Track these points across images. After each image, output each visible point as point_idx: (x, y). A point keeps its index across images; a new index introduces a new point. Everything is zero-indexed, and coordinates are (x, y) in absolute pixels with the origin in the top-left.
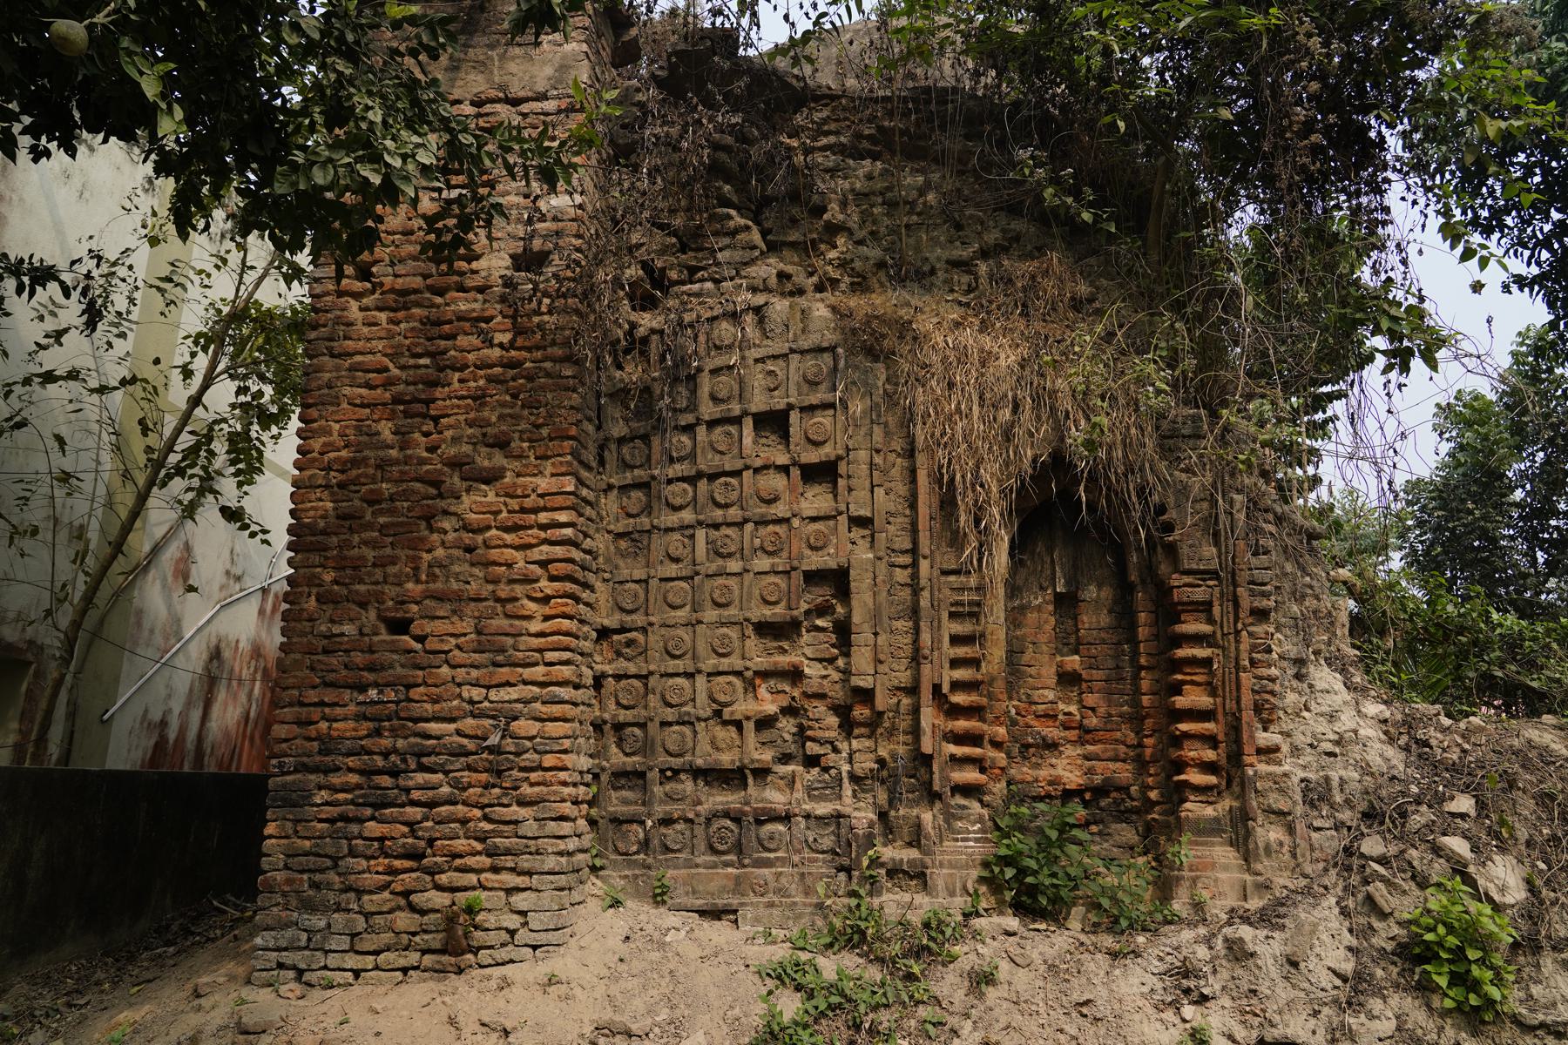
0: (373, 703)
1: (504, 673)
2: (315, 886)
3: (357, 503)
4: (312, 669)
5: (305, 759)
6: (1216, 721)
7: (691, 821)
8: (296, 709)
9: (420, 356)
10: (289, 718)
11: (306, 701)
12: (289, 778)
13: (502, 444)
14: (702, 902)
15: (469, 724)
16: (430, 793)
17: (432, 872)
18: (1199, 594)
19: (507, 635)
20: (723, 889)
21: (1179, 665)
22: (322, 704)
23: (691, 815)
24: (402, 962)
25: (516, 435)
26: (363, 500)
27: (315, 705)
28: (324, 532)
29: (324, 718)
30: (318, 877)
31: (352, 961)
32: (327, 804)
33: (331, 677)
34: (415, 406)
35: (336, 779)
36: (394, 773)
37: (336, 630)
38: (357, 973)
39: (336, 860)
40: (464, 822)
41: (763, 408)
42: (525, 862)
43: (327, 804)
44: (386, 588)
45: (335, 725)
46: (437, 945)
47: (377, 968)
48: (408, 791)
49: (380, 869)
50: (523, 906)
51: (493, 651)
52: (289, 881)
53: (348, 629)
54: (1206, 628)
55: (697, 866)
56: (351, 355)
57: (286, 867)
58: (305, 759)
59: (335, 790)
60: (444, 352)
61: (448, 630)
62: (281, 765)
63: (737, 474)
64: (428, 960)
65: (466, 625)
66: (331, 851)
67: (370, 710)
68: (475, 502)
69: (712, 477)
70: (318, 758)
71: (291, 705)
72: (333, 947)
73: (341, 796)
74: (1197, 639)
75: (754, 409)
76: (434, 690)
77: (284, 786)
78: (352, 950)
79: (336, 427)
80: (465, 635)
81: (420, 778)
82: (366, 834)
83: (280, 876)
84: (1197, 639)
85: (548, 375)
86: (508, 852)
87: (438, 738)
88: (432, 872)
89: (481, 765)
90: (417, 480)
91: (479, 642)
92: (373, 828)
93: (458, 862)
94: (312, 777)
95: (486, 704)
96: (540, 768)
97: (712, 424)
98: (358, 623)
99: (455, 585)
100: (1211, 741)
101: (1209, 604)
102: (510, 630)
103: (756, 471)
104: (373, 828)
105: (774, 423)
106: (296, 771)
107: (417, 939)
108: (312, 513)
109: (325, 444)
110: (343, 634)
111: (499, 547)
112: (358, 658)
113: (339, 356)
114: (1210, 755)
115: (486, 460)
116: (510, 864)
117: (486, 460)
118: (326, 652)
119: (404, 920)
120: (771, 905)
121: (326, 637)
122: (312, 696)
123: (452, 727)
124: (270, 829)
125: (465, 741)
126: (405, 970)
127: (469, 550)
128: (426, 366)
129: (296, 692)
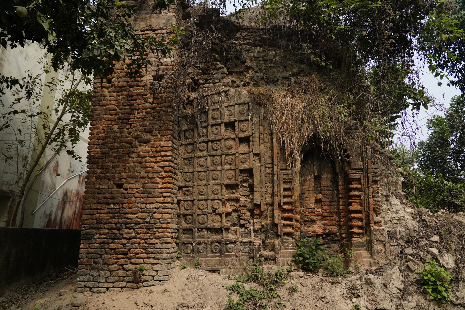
0: (112, 208)
1: (151, 200)
2: (95, 263)
3: (107, 149)
4: (94, 198)
5: (92, 225)
7: (206, 244)
9: (126, 106)
10: (87, 213)
11: (92, 208)
12: (87, 231)
13: (150, 132)
16: (129, 235)
17: (130, 259)
19: (152, 188)
20: (216, 264)
22: (97, 209)
23: (206, 242)
24: (121, 285)
25: (154, 129)
26: (109, 148)
28: (97, 158)
30: (96, 260)
31: (106, 285)
32: (98, 238)
33: (100, 201)
34: (124, 121)
35: (101, 231)
36: (118, 229)
37: (101, 187)
38: (107, 289)
39: (101, 255)
41: (227, 121)
42: (157, 256)
43: (98, 238)
44: (116, 175)
45: (101, 215)
47: (113, 287)
48: (122, 235)
50: (157, 269)
52: (87, 261)
53: (105, 187)
55: (208, 257)
56: (105, 105)
57: (87, 257)
58: (92, 225)
59: (101, 234)
61: (132, 186)
62: (85, 227)
63: (220, 140)
64: (128, 285)
65: (140, 186)
67: (111, 211)
68: (142, 149)
69: (212, 142)
70: (96, 225)
71: (88, 209)
72: (100, 281)
73: (103, 236)
74: (357, 189)
75: (225, 121)
77: (86, 233)
78: (106, 282)
79: (101, 127)
80: (139, 188)
81: (126, 231)
82: (110, 247)
83: (85, 260)
84: (357, 189)
86: (152, 253)
87: (131, 219)
88: (130, 259)
89: (144, 227)
90: (125, 143)
91: (143, 191)
92: (112, 246)
93: (137, 256)
94: (94, 231)
97: (212, 126)
98: (107, 185)
99: (136, 174)
100: (361, 220)
101: (360, 179)
103: (226, 140)
104: (112, 246)
105: (231, 125)
106: (89, 229)
107: (125, 278)
108: (94, 152)
109: (98, 132)
110: (103, 188)
112: (108, 195)
113: (102, 106)
114: (360, 224)
115: (145, 136)
116: (153, 256)
117: (145, 136)
118: (98, 193)
119: (121, 273)
120: (230, 268)
121: (98, 189)
122: (94, 206)
123: (136, 216)
124: (82, 246)
125: (139, 220)
126: (122, 288)
127: (141, 163)
128: (128, 109)
129: (89, 205)
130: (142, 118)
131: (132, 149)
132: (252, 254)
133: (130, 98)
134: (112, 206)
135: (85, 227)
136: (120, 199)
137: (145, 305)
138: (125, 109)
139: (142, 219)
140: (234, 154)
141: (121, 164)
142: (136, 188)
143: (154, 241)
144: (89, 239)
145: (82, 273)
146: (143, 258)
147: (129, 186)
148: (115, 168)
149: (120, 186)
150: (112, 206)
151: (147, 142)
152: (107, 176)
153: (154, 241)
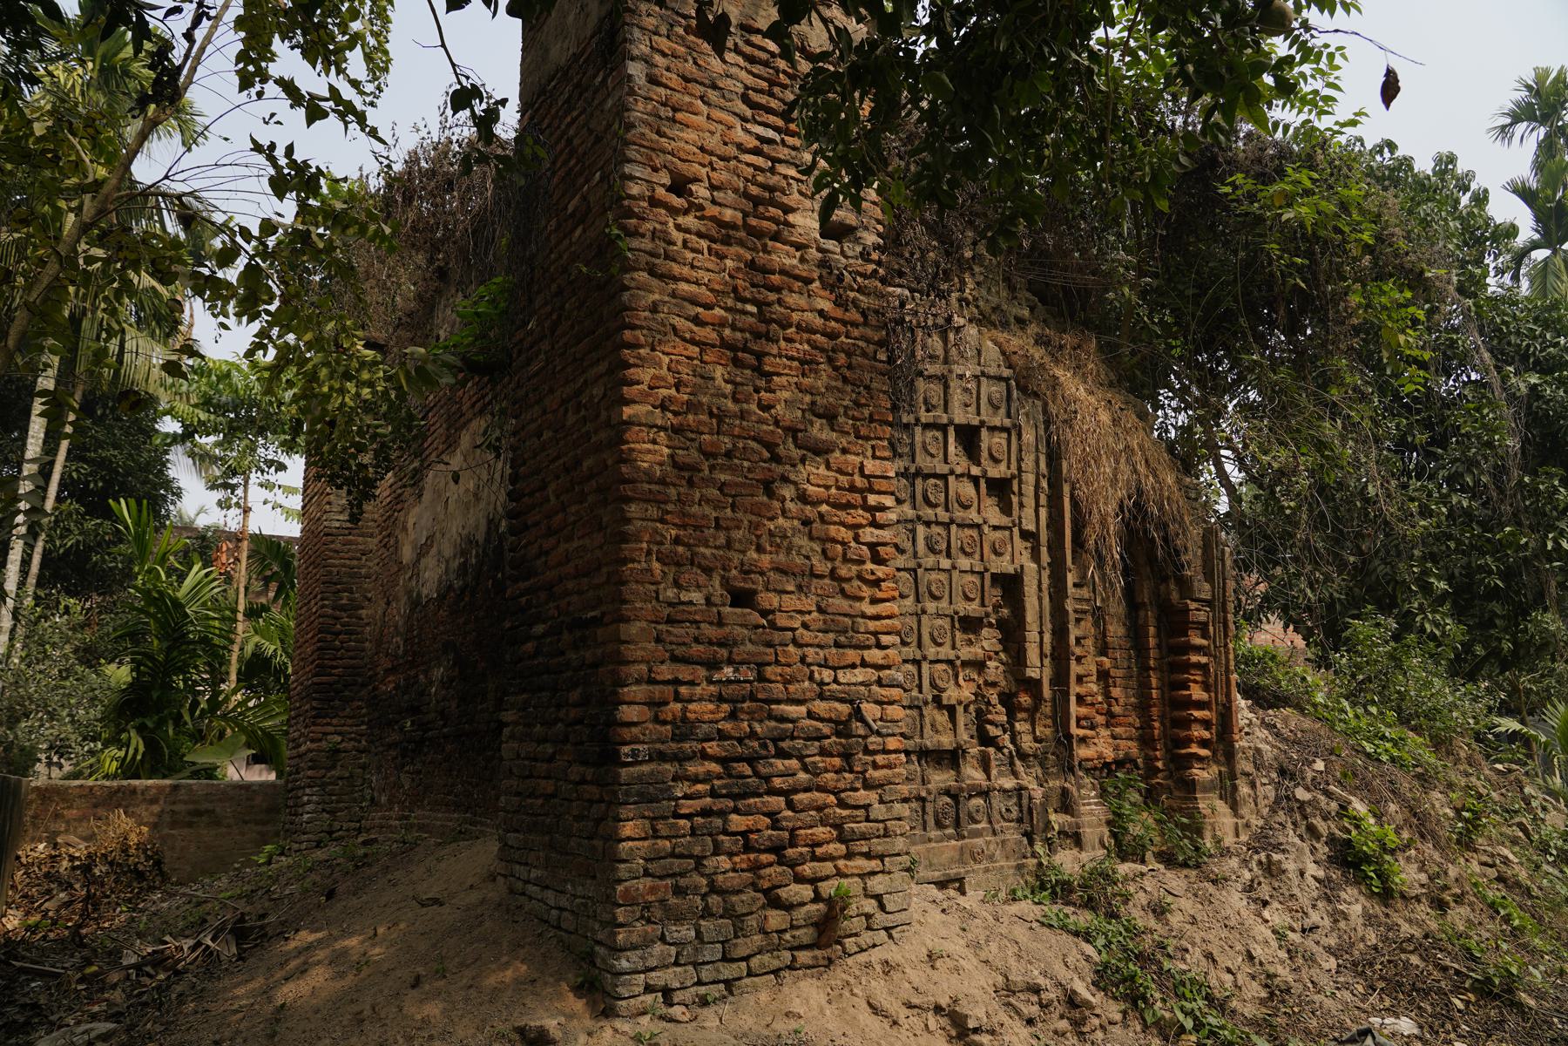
0: (729, 682)
1: (852, 655)
2: (679, 891)
3: (695, 454)
4: (658, 640)
5: (658, 746)
6: (1210, 710)
7: (923, 800)
8: (644, 687)
9: (745, 301)
10: (640, 697)
11: (659, 678)
12: (646, 768)
13: (830, 417)
14: (937, 874)
15: (820, 707)
16: (790, 780)
17: (793, 865)
18: (1202, 616)
19: (845, 615)
20: (952, 860)
21: (1188, 667)
22: (677, 682)
23: (924, 794)
24: (776, 964)
25: (842, 410)
26: (700, 450)
27: (667, 682)
28: (662, 482)
29: (677, 698)
30: (683, 882)
31: (728, 971)
32: (686, 797)
33: (679, 651)
34: (748, 356)
35: (693, 768)
36: (751, 760)
37: (684, 597)
38: (728, 984)
39: (699, 860)
40: (819, 809)
41: (964, 421)
42: (878, 846)
43: (686, 797)
44: (731, 554)
45: (691, 707)
46: (806, 940)
47: (750, 975)
48: (768, 779)
49: (744, 866)
50: (879, 889)
51: (844, 634)
52: (653, 890)
53: (697, 597)
54: (1205, 642)
55: (930, 840)
56: (676, 279)
57: (647, 873)
58: (658, 746)
59: (696, 780)
60: (769, 304)
61: (792, 606)
62: (634, 753)
63: (944, 477)
64: (804, 957)
65: (809, 603)
66: (697, 850)
67: (728, 691)
68: (815, 476)
69: (927, 477)
70: (674, 745)
71: (638, 682)
72: (707, 958)
73: (700, 787)
74: (1199, 649)
75: (957, 421)
76: (788, 670)
77: (640, 778)
78: (726, 959)
79: (666, 359)
80: (810, 613)
81: (780, 764)
82: (733, 828)
83: (644, 884)
84: (1199, 649)
85: (864, 354)
86: (864, 837)
87: (793, 721)
88: (793, 865)
89: (835, 751)
90: (754, 439)
91: (825, 622)
92: (737, 822)
93: (819, 851)
94: (668, 766)
95: (835, 686)
96: (886, 752)
97: (927, 426)
98: (705, 591)
99: (799, 560)
100: (1206, 724)
101: (1206, 624)
102: (849, 611)
103: (958, 476)
104: (737, 822)
105: (969, 437)
106: (651, 760)
107: (787, 936)
108: (649, 457)
109: (654, 377)
110: (691, 603)
111: (835, 523)
112: (709, 631)
113: (661, 277)
114: (1206, 735)
115: (820, 431)
116: (865, 849)
117: (820, 431)
118: (670, 621)
119: (776, 919)
120: (987, 870)
121: (670, 604)
122: (665, 671)
123: (803, 709)
124: (628, 829)
125: (820, 725)
126: (776, 972)
127: (806, 523)
128: (752, 314)
129: (644, 667)
130: (802, 362)
131: (779, 469)
132: (1030, 825)
133: (759, 278)
134: (728, 671)
135: (634, 753)
136: (750, 647)
137: (916, 1011)
138: (745, 313)
139: (830, 720)
140: (978, 526)
141: (746, 519)
142: (800, 612)
143: (862, 796)
144: (651, 802)
145: (635, 939)
146: (832, 858)
147: (772, 600)
148: (728, 529)
149: (742, 598)
150: (728, 671)
151: (820, 450)
152: (704, 556)
153: (862, 796)
